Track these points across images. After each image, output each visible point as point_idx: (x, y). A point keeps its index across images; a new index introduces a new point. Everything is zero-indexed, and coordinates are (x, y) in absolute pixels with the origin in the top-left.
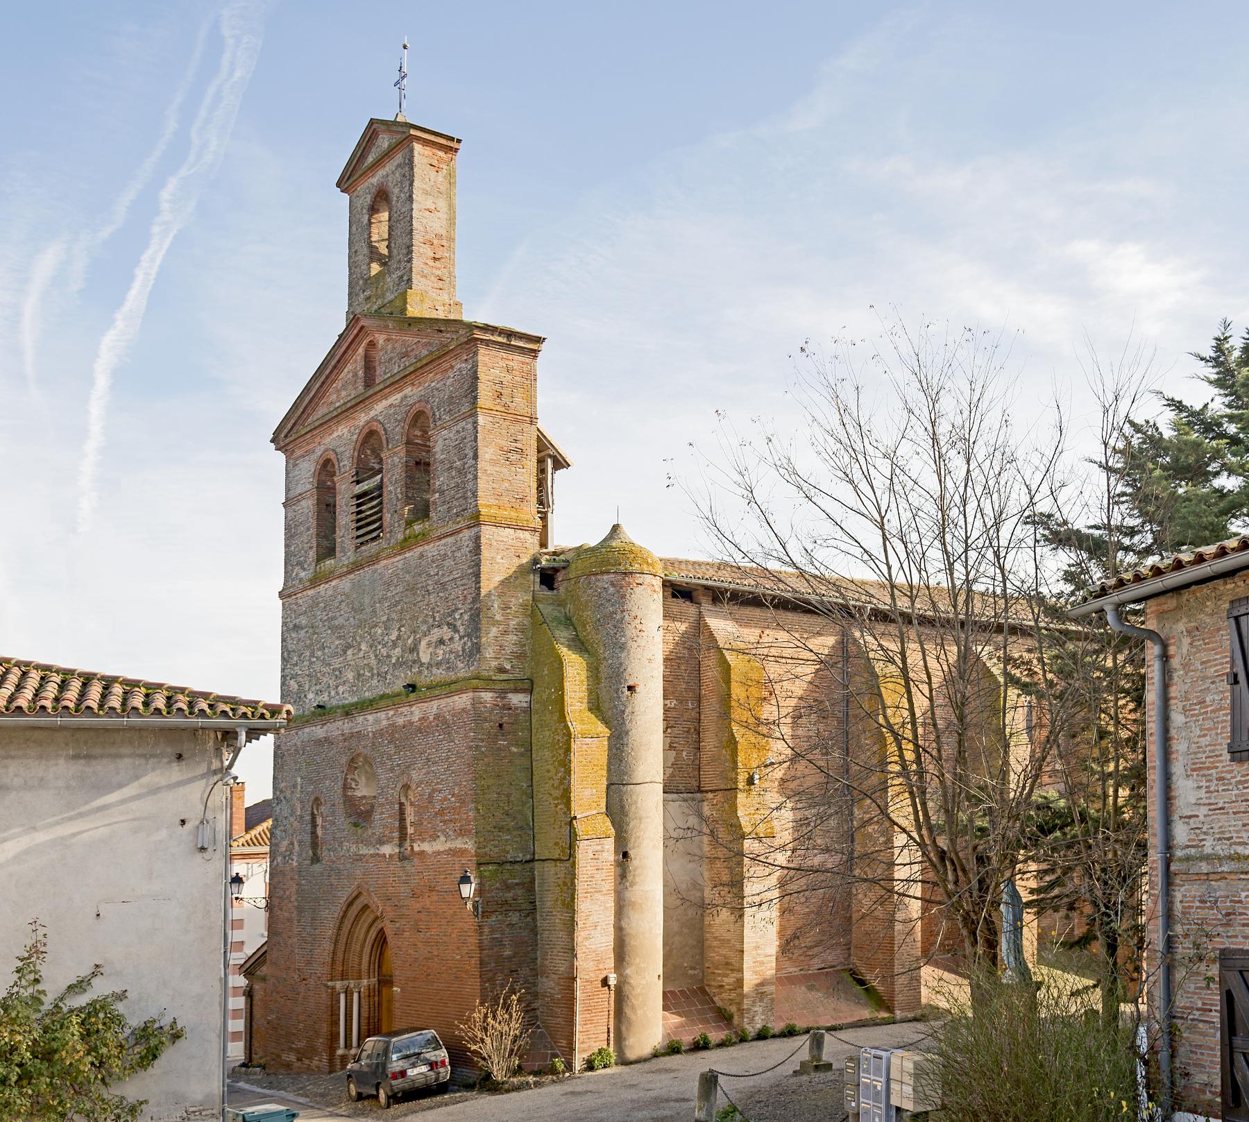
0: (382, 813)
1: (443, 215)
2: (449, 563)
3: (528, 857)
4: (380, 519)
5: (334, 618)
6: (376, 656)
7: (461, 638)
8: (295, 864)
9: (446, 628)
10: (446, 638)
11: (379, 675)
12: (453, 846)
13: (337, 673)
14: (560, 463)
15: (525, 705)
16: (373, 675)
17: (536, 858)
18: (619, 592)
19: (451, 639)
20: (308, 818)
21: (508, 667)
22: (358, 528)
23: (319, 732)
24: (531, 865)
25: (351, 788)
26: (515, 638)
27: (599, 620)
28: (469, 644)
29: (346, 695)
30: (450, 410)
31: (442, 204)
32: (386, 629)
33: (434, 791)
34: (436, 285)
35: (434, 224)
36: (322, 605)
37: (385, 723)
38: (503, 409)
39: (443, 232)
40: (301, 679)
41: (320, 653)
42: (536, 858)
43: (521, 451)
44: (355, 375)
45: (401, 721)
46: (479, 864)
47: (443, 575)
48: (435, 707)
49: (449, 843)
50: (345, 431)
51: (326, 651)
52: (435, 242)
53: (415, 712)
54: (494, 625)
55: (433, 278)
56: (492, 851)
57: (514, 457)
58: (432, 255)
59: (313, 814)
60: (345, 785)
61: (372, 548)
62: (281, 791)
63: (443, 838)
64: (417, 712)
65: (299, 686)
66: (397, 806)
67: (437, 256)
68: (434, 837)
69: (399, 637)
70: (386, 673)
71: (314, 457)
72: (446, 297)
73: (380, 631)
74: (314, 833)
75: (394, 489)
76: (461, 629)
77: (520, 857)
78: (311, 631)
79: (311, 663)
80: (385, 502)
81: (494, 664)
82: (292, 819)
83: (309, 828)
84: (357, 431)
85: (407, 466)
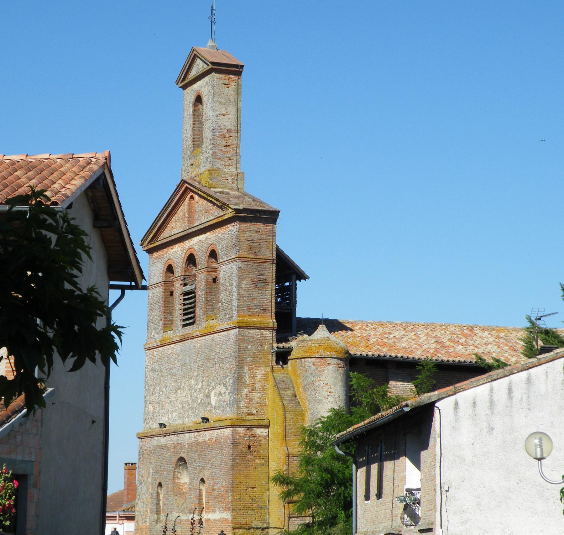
0: (191, 495)
1: (232, 116)
2: (224, 347)
3: (265, 526)
4: (194, 312)
5: (172, 369)
6: (191, 396)
7: (229, 393)
8: (148, 524)
9: (222, 386)
10: (223, 392)
11: (192, 409)
12: (222, 517)
13: (172, 404)
14: (302, 276)
15: (265, 434)
16: (189, 408)
17: (270, 526)
18: (317, 369)
19: (225, 393)
20: (155, 495)
21: (254, 411)
22: (184, 315)
23: (162, 440)
24: (267, 530)
25: (178, 478)
26: (259, 394)
27: (306, 385)
28: (232, 398)
29: (176, 418)
30: (226, 254)
31: (232, 110)
32: (196, 381)
33: (215, 483)
34: (227, 164)
35: (226, 124)
36: (166, 358)
37: (193, 439)
38: (253, 256)
39: (232, 128)
40: (154, 405)
41: (164, 389)
42: (270, 526)
43: (265, 281)
44: (184, 214)
45: (200, 440)
46: (234, 528)
47: (222, 354)
48: (216, 433)
49: (220, 515)
50: (179, 249)
51: (167, 388)
52: (227, 135)
53: (207, 435)
54: (245, 387)
55: (225, 160)
56: (242, 520)
57: (260, 285)
58: (225, 144)
59: (158, 492)
60: (174, 475)
61: (190, 330)
62: (142, 477)
63: (218, 512)
64: (208, 435)
65: (154, 409)
66: (198, 491)
67: (228, 144)
68: (214, 511)
69: (202, 387)
70: (195, 408)
71: (164, 261)
72: (234, 170)
73: (193, 382)
74: (158, 504)
75: (200, 295)
76: (229, 388)
77: (260, 525)
78: (160, 374)
79: (160, 395)
80: (197, 301)
81: (245, 410)
82: (147, 495)
83: (155, 501)
84: (185, 251)
85: (207, 282)
